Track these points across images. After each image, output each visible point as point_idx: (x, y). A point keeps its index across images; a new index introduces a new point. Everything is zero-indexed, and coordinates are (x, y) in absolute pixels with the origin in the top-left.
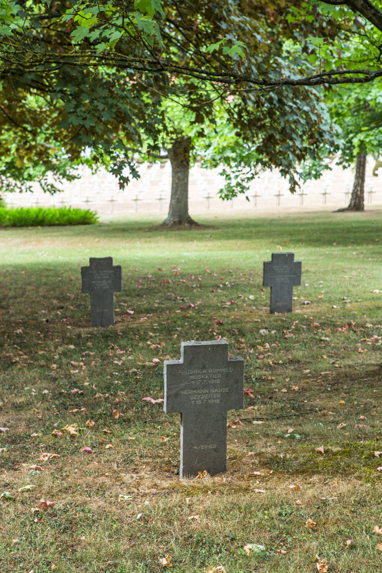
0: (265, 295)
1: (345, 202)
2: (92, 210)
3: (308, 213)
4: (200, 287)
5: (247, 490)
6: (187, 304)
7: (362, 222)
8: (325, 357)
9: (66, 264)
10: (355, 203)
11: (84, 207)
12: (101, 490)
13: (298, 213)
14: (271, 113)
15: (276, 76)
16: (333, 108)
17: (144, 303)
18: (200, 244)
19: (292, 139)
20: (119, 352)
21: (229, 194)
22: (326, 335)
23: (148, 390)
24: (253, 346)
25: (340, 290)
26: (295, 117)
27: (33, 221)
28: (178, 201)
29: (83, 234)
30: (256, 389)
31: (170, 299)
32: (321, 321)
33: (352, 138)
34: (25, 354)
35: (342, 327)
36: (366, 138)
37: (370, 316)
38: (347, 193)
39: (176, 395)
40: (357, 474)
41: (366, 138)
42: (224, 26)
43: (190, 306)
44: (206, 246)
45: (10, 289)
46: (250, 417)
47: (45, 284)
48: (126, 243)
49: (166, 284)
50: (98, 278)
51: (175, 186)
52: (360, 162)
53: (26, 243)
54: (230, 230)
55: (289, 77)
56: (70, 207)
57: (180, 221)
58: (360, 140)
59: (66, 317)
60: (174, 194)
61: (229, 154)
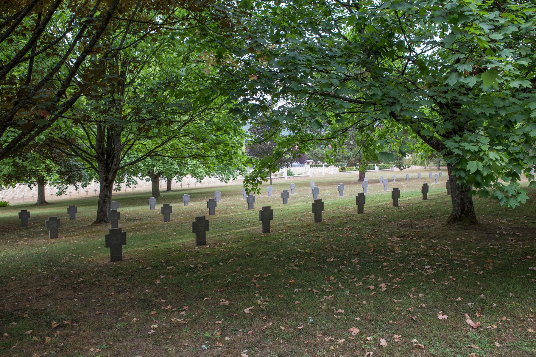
2: (7, 201)
9: (5, 217)
17: (35, 221)
21: (60, 194)
28: (41, 196)
29: (6, 209)
57: (42, 202)
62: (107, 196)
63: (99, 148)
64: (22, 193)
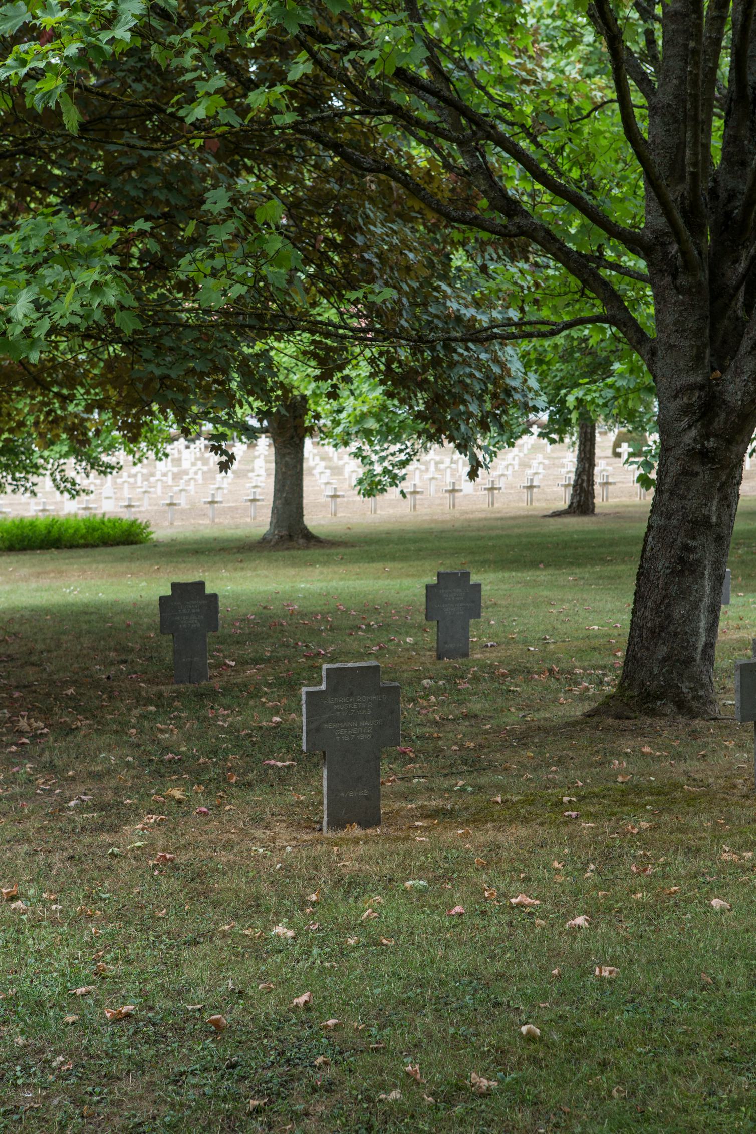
0: (430, 638)
1: (562, 499)
2: (142, 519)
3: (502, 519)
4: (332, 629)
5: (406, 839)
6: (315, 651)
7: (589, 532)
8: (513, 710)
9: (115, 603)
10: (579, 502)
11: (127, 516)
12: (228, 845)
13: (486, 519)
14: (436, 362)
15: (438, 309)
16: (532, 352)
17: (249, 651)
18: (325, 570)
19: (464, 402)
20: (222, 712)
21: (371, 487)
22: (516, 685)
23: (272, 752)
24: (413, 700)
25: (541, 627)
26: (468, 370)
27: (42, 541)
28: (287, 502)
29: (131, 559)
30: (418, 747)
31: (287, 646)
32: (511, 667)
33: (566, 395)
34: (87, 718)
35: (539, 674)
36: (586, 394)
37: (580, 659)
38: (566, 486)
39: (318, 730)
40: (538, 821)
41: (586, 394)
42: (360, 240)
43: (319, 654)
44: (335, 572)
45: (36, 641)
46: (409, 775)
47: (89, 632)
48: (204, 571)
49: (278, 628)
50: (185, 611)
51: (280, 477)
52: (586, 433)
53: (38, 575)
54: (373, 548)
55: (459, 310)
56: (104, 515)
57: (290, 534)
58: (577, 398)
59: (135, 672)
61: (372, 424)
62: (706, 523)
63: (676, 167)
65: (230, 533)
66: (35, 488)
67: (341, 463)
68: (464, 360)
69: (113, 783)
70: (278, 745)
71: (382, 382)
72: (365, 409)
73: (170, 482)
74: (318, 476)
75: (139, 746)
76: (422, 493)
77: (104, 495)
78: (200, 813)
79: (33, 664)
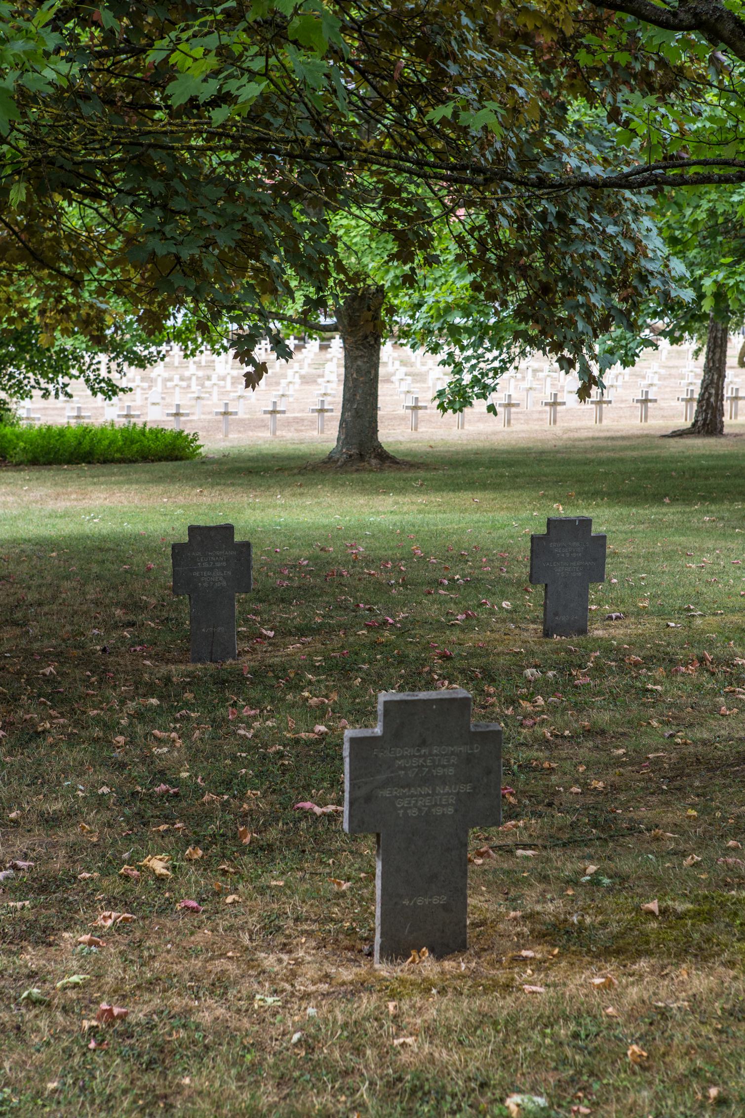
3: (612, 438)
5: (508, 987)
8: (655, 723)
9: (137, 538)
10: (705, 420)
11: (171, 426)
12: (220, 986)
13: (593, 439)
14: (545, 241)
17: (294, 615)
19: (584, 290)
20: (248, 712)
21: (456, 399)
22: (656, 681)
23: (307, 787)
26: (590, 248)
28: (358, 415)
29: (171, 479)
30: (521, 786)
34: (62, 715)
35: (686, 665)
38: (689, 400)
39: (368, 799)
42: (453, 70)
43: (385, 623)
46: (509, 841)
47: (98, 577)
49: (337, 579)
50: (206, 565)
57: (361, 453)
59: (141, 643)
60: (348, 401)
64: (232, 394)
65: (291, 448)
66: (68, 389)
67: (424, 369)
68: (585, 234)
69: (71, 836)
70: (319, 775)
71: (471, 269)
72: (450, 299)
73: (229, 387)
74: (397, 383)
75: (122, 766)
76: (518, 405)
77: (150, 401)
78: (187, 908)
79: (15, 624)
